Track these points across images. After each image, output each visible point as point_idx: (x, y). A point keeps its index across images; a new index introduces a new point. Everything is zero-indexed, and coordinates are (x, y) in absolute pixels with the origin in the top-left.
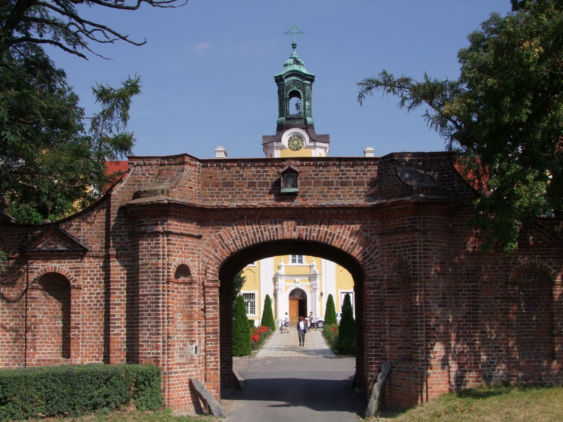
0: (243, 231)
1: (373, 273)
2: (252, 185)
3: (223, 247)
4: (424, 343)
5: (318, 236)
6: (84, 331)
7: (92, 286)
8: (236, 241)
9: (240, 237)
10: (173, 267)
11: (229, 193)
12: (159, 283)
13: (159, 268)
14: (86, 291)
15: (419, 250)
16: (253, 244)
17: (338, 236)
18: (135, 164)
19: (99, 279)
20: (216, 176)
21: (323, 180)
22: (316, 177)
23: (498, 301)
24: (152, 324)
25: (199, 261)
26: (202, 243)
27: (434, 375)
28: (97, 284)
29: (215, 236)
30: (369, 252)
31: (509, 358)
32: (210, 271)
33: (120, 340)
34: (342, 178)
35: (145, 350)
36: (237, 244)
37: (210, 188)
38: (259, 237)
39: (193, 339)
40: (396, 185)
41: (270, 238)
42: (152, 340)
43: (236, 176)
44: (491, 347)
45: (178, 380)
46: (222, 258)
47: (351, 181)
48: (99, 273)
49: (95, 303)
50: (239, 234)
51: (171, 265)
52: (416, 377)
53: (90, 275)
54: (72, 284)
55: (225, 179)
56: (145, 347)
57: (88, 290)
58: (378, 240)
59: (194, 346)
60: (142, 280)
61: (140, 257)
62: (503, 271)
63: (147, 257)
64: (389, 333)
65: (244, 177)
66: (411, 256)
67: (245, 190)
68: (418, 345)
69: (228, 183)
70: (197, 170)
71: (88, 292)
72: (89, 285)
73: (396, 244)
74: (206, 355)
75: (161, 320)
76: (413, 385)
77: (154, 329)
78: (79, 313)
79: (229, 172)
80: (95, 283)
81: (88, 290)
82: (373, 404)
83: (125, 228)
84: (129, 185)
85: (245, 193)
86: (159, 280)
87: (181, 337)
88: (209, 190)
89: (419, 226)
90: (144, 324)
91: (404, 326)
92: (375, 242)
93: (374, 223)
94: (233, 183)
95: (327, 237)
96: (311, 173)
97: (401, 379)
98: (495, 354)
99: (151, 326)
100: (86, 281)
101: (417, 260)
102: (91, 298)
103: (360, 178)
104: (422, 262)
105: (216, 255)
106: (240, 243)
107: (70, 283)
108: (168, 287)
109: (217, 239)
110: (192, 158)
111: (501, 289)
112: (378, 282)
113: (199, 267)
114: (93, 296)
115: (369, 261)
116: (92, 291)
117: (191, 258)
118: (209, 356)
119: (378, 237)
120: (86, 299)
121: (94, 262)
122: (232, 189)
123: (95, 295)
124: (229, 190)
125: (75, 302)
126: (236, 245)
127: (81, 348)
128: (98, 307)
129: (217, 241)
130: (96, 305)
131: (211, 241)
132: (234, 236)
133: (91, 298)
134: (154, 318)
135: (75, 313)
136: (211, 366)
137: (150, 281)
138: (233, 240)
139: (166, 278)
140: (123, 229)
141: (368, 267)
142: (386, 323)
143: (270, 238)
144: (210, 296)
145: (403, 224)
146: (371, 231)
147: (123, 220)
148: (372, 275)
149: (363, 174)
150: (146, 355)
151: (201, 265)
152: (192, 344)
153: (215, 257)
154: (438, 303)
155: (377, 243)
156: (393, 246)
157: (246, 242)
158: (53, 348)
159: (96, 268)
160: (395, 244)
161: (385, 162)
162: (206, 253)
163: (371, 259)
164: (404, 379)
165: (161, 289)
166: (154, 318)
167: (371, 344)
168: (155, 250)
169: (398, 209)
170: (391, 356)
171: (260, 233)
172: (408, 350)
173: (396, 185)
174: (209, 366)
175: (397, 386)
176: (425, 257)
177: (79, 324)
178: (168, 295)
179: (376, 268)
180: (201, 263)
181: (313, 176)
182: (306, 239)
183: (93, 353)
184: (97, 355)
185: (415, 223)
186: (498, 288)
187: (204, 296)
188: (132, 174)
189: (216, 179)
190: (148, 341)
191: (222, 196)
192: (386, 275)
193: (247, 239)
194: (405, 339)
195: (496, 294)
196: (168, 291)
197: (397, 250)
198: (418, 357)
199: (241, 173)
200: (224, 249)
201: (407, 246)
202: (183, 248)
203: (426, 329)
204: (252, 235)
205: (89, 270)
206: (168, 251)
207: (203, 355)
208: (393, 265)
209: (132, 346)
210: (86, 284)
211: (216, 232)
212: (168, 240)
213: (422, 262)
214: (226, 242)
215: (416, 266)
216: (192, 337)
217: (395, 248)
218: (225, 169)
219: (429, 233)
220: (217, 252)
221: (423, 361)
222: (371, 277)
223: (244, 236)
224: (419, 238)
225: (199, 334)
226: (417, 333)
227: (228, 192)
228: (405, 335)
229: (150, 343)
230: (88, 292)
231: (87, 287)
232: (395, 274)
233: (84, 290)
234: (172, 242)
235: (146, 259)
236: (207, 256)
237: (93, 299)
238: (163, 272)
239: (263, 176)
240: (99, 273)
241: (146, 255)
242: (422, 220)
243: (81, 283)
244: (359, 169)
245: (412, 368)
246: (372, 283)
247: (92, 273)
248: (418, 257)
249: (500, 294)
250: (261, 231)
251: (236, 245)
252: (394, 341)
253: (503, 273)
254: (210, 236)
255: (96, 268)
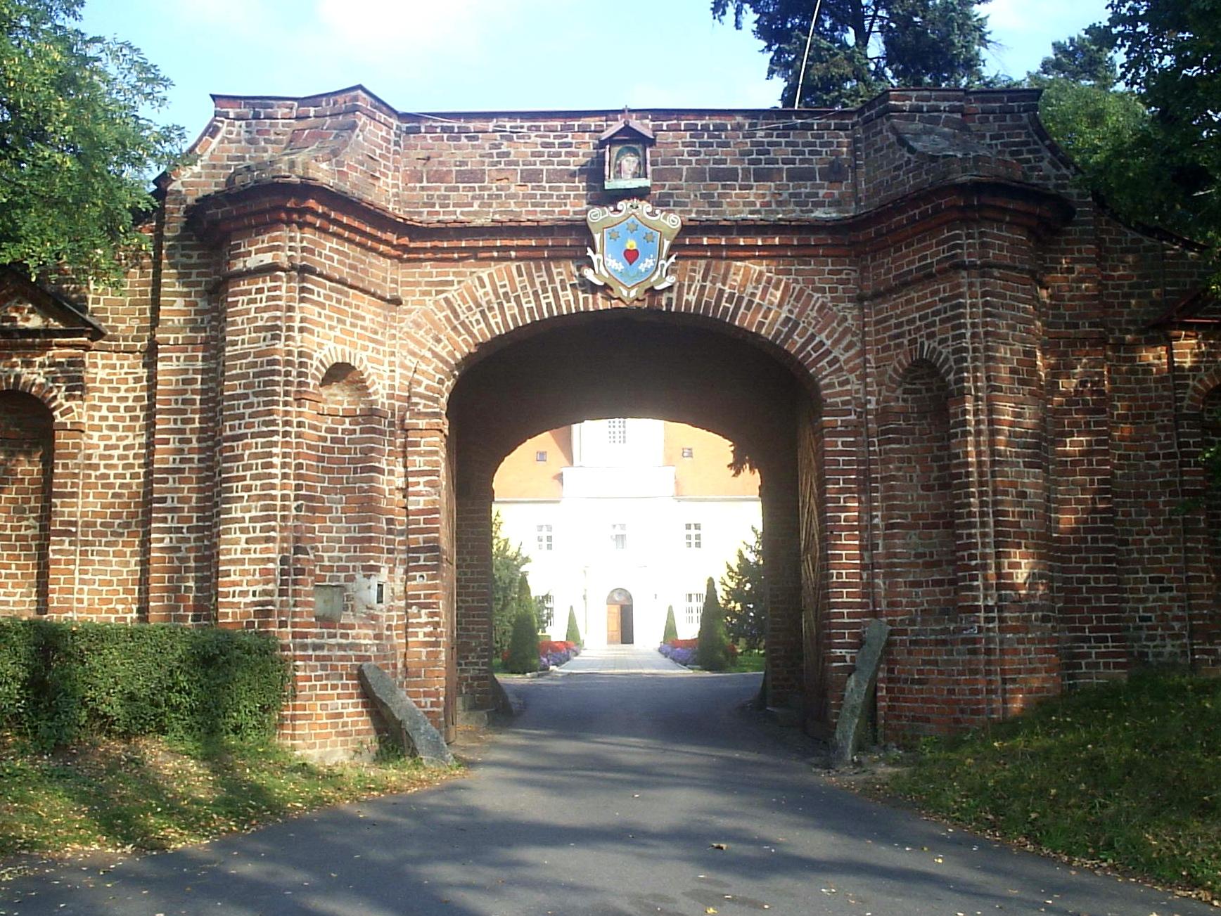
0: (508, 289)
1: (839, 394)
2: (531, 176)
3: (454, 329)
4: (991, 562)
5: (699, 302)
6: (86, 543)
7: (113, 428)
8: (489, 315)
9: (500, 304)
10: (316, 363)
11: (474, 198)
12: (276, 403)
13: (275, 362)
14: (95, 441)
15: (972, 316)
16: (534, 322)
17: (750, 302)
18: (232, 115)
19: (133, 409)
20: (441, 156)
21: (712, 166)
22: (694, 159)
23: (1157, 463)
24: (253, 514)
25: (391, 363)
26: (402, 320)
27: (1021, 647)
28: (128, 423)
29: (436, 302)
30: (829, 343)
31: (1190, 607)
32: (421, 390)
33: (176, 564)
34: (759, 161)
35: (234, 584)
36: (492, 322)
37: (425, 184)
38: (549, 305)
39: (372, 563)
40: (898, 168)
41: (577, 307)
42: (253, 556)
43: (491, 155)
44: (1143, 581)
45: (324, 668)
46: (454, 357)
47: (780, 170)
48: (131, 395)
49: (120, 471)
50: (497, 297)
51: (311, 357)
52: (974, 652)
53: (110, 399)
54: (59, 419)
55: (463, 163)
56: (233, 578)
57: (101, 438)
58: (850, 313)
59: (374, 582)
60: (232, 397)
61: (228, 338)
62: (1165, 388)
63: (246, 337)
64: (885, 547)
65: (512, 158)
66: (950, 335)
67: (513, 189)
68: (976, 568)
69: (471, 172)
70: (393, 138)
71: (102, 444)
72: (104, 424)
73: (903, 314)
74: (409, 606)
75: (279, 503)
76: (961, 673)
77: (258, 525)
78: (73, 495)
79: (473, 146)
80: (122, 419)
81: (101, 438)
82: (848, 729)
83: (198, 275)
84: (214, 167)
85: (514, 196)
86: (274, 393)
87: (340, 559)
88: (423, 188)
89: (970, 255)
90: (233, 515)
91: (926, 526)
92: (845, 319)
93: (840, 272)
94: (483, 172)
95: (724, 303)
96: (681, 148)
97: (925, 663)
98: (1151, 597)
99: (252, 520)
100: (97, 414)
101: (966, 343)
102: (111, 457)
103: (802, 161)
104: (981, 347)
105: (438, 349)
106: (499, 319)
107: (53, 418)
108: (300, 414)
109: (442, 310)
110: (380, 104)
111: (1162, 434)
112: (853, 417)
113: (393, 378)
114: (115, 453)
115: (830, 364)
116: (113, 441)
117: (369, 353)
118: (414, 609)
119: (850, 305)
120: (95, 461)
121: (122, 366)
122: (481, 189)
123: (121, 451)
124: (473, 189)
125: (65, 466)
126: (488, 325)
127: (77, 587)
128: (128, 480)
129: (441, 315)
130: (123, 476)
131: (425, 314)
132: (484, 304)
133: (111, 457)
134: (260, 498)
135: (62, 495)
136: (421, 635)
137: (252, 399)
138: (482, 312)
139: (293, 389)
140: (194, 278)
141: (826, 381)
142: (876, 521)
143: (577, 307)
144: (419, 454)
145: (925, 257)
146: (832, 290)
147: (195, 254)
148: (838, 400)
149: (811, 153)
150: (236, 599)
151: (397, 375)
152: (369, 577)
153: (435, 354)
154: (1024, 456)
155: (850, 321)
156: (893, 321)
157: (514, 317)
158: (10, 589)
159: (126, 381)
160: (898, 316)
161: (868, 120)
162: (412, 346)
163: (836, 360)
164: (936, 663)
165: (279, 419)
166: (260, 498)
167: (839, 575)
168: (266, 315)
169: (912, 220)
170: (890, 604)
171: (550, 294)
172: (937, 589)
173: (898, 168)
174: (416, 634)
175: (913, 681)
176: (987, 334)
177: (75, 524)
178: (298, 435)
179: (847, 382)
180: (398, 370)
181: (686, 157)
182: (669, 310)
183: (110, 601)
184: (120, 607)
185: (960, 246)
186: (1155, 432)
187: (405, 457)
188: (222, 142)
189: (440, 163)
190: (242, 562)
191: (455, 205)
192: (873, 399)
193: (516, 311)
194: (928, 559)
195: (1151, 447)
196: (300, 425)
197: (906, 328)
198: (976, 598)
199: (504, 149)
200: (460, 335)
201: (935, 314)
202: (348, 320)
203: (997, 523)
204: (532, 298)
205: (106, 386)
206: (302, 320)
207: (399, 609)
208: (895, 370)
209: (208, 579)
210: (96, 422)
211: (438, 293)
212: (302, 290)
213: (981, 347)
214: (462, 317)
215: (965, 360)
216: (370, 558)
217: (898, 325)
218: (464, 141)
219: (996, 273)
220: (438, 341)
221: (988, 609)
222: (836, 404)
223: (509, 301)
224: (971, 285)
225: (390, 551)
226: (970, 536)
227: (470, 194)
228: (927, 551)
229: (246, 567)
230: (102, 444)
231: (99, 429)
232: (899, 391)
233: (90, 437)
234: (315, 297)
235: (243, 343)
236: (414, 354)
237: (115, 461)
238: (288, 374)
239: (559, 155)
240: (131, 395)
241: (243, 332)
242: (977, 241)
243: (84, 420)
244: (800, 141)
245: (959, 630)
246: (839, 419)
247: (115, 396)
248: (968, 335)
249: (1161, 447)
250: (554, 290)
251: (488, 325)
252: (901, 565)
253: (1166, 393)
254: (422, 303)
255: (126, 381)
